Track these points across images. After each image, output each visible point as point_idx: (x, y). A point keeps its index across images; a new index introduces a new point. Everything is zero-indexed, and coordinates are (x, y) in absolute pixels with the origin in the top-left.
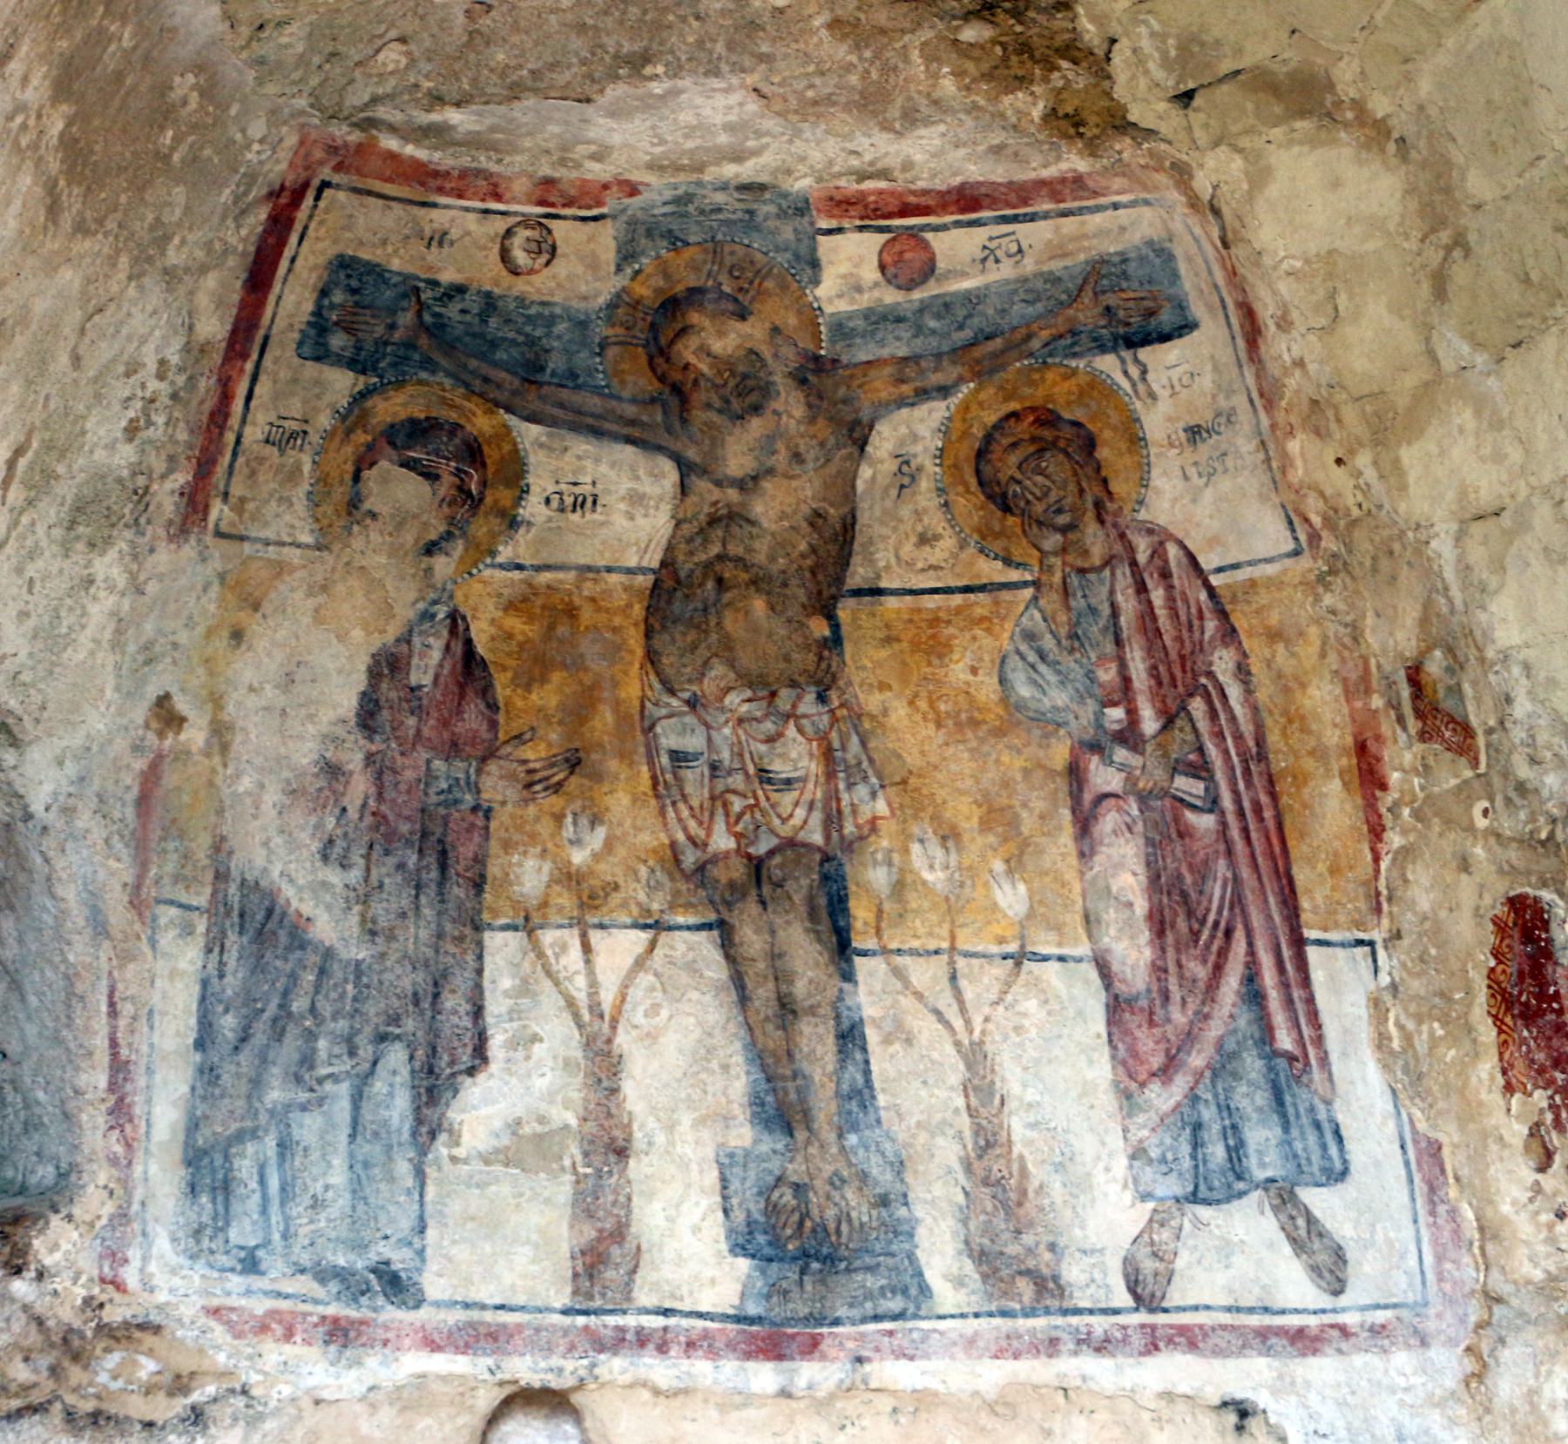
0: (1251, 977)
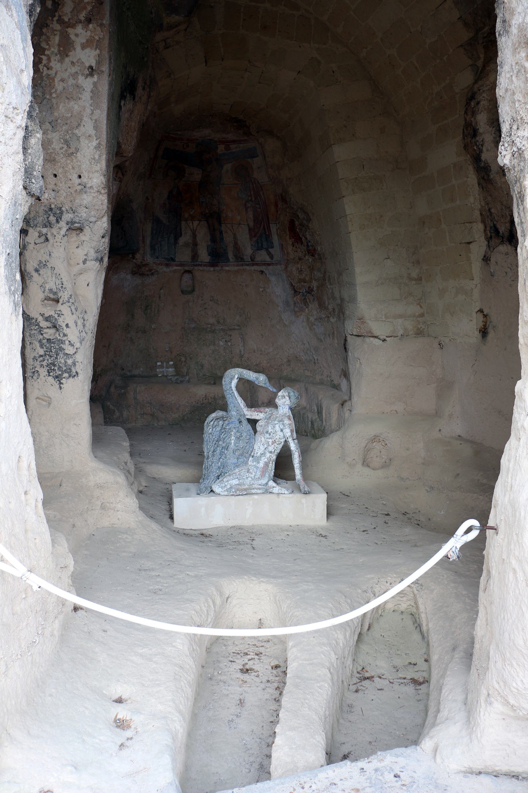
0: (264, 226)
